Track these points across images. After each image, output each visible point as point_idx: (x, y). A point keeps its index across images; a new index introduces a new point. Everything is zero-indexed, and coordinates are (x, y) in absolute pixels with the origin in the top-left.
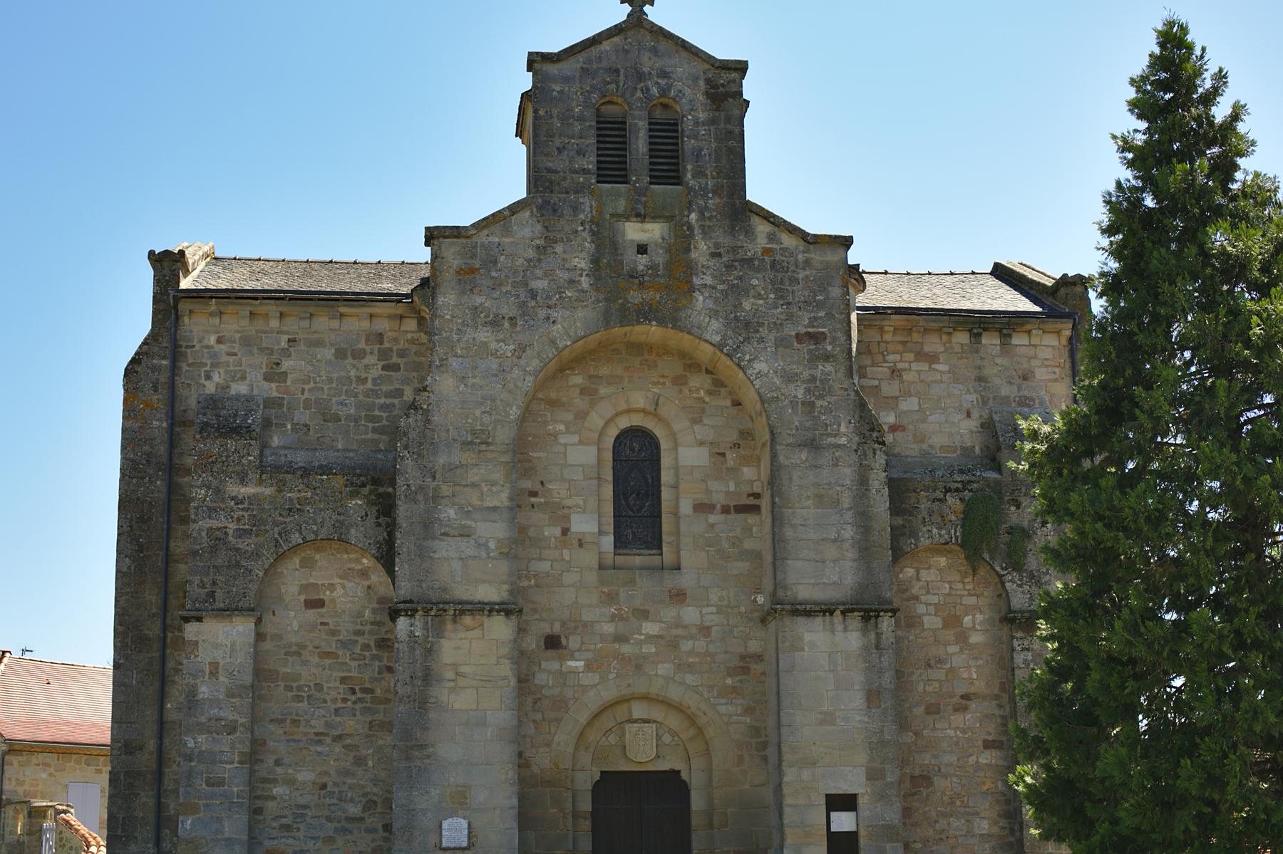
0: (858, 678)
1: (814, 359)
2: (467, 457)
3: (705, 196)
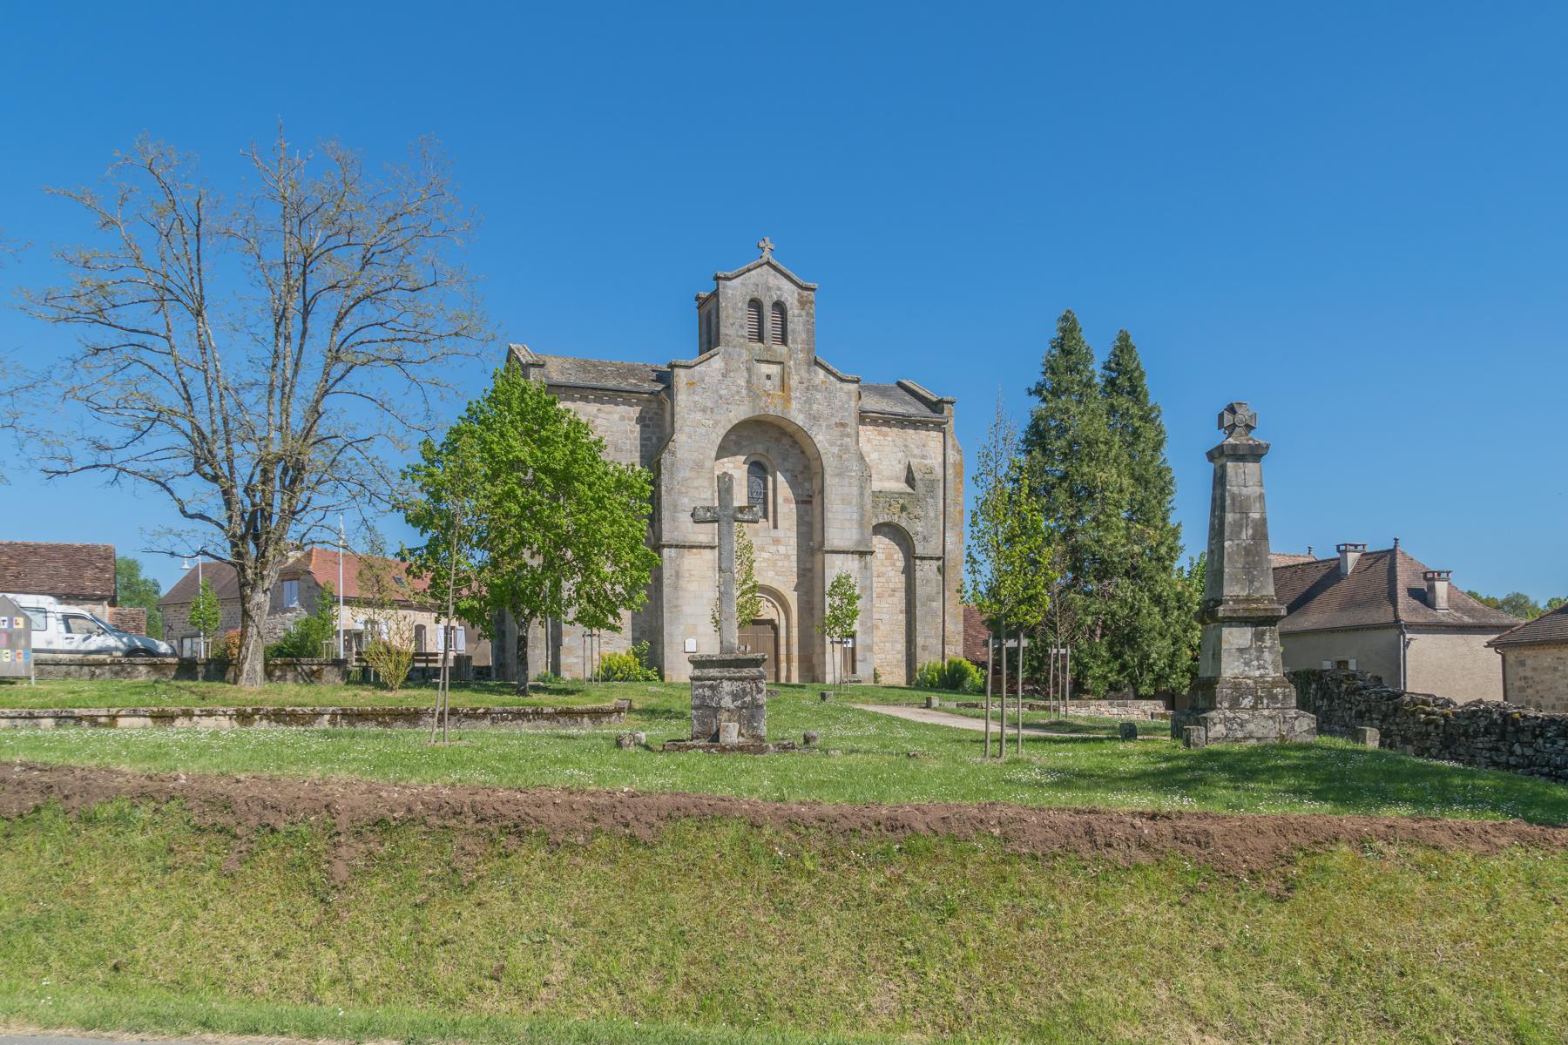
1: (843, 436)
2: (693, 474)
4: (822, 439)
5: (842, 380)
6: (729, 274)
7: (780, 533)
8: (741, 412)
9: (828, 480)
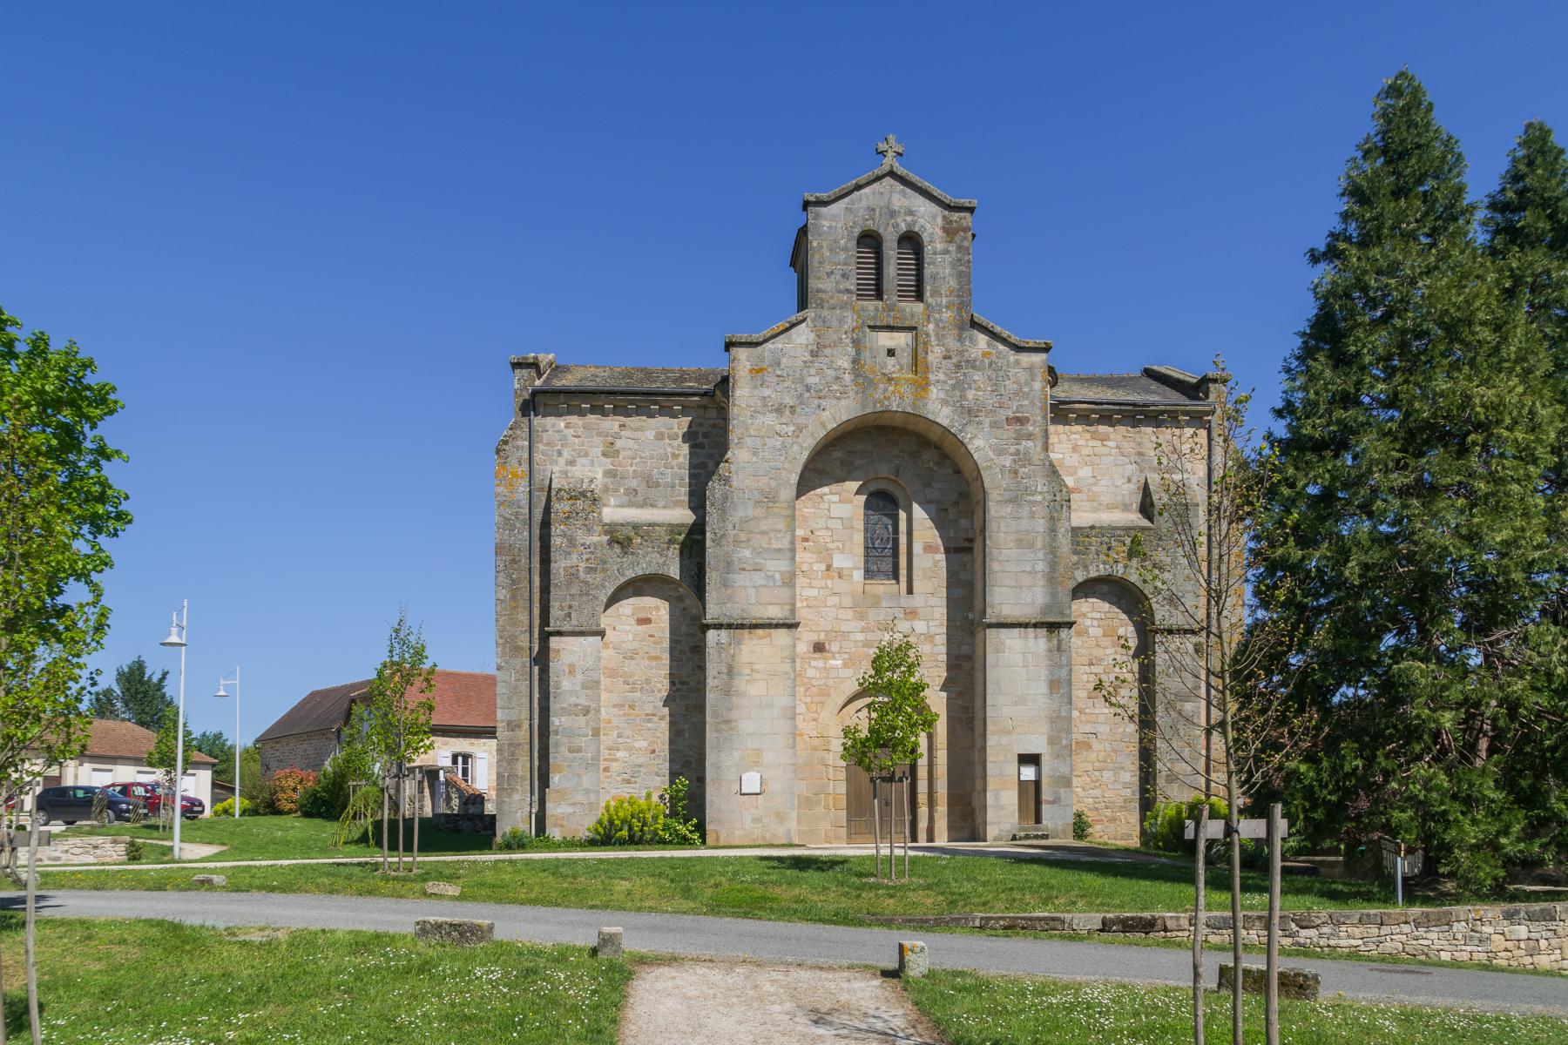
0: (1044, 673)
1: (1019, 438)
2: (760, 512)
3: (940, 312)
4: (981, 444)
5: (1018, 349)
6: (824, 196)
7: (917, 601)
8: (839, 411)
9: (994, 510)
